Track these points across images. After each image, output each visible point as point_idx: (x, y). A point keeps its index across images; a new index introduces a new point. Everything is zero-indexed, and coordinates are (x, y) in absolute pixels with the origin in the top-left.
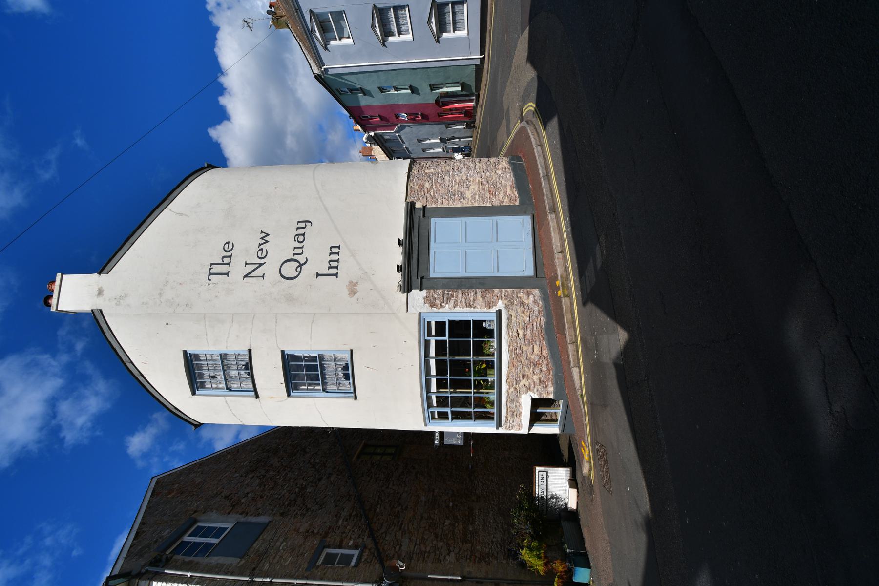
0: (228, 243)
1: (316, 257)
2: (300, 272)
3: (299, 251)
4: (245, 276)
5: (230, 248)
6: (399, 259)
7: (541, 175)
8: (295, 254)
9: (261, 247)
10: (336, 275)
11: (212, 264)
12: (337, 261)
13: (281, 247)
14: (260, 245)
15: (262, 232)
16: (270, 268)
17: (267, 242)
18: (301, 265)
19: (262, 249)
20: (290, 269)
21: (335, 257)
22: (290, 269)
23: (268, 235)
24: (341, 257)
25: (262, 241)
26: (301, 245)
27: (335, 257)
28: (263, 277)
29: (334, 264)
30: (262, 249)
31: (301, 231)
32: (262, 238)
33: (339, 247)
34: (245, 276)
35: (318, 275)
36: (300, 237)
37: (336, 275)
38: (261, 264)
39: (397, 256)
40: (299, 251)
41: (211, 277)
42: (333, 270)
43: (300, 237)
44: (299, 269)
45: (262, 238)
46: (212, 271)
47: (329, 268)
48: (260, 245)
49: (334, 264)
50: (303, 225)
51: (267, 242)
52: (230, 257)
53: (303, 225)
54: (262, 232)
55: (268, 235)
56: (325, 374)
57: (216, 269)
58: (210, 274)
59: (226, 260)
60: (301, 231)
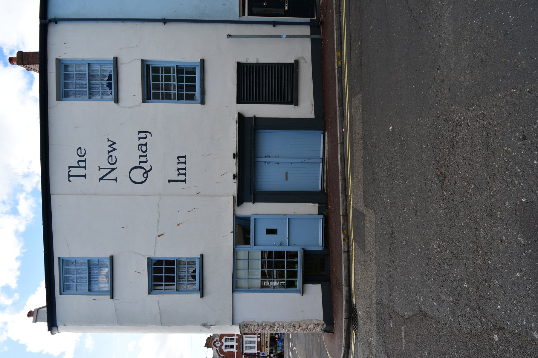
0: (80, 148)
1: (163, 166)
2: (147, 178)
3: (144, 159)
4: (101, 179)
5: (114, 162)
6: (234, 170)
7: (340, 178)
8: (140, 162)
9: (110, 154)
10: (185, 181)
11: (70, 167)
12: (185, 169)
13: (128, 155)
14: (109, 152)
15: (108, 140)
16: (122, 171)
17: (115, 149)
18: (147, 172)
19: (111, 156)
20: (138, 175)
21: (182, 166)
22: (138, 175)
23: (114, 143)
24: (187, 166)
25: (110, 149)
26: (145, 154)
27: (182, 166)
28: (116, 180)
29: (182, 172)
30: (111, 156)
31: (143, 142)
32: (110, 146)
33: (185, 157)
34: (101, 179)
35: (169, 181)
36: (143, 148)
37: (185, 181)
38: (113, 169)
39: (232, 166)
40: (144, 159)
41: (71, 178)
42: (181, 176)
43: (143, 148)
44: (145, 175)
45: (110, 146)
46: (71, 174)
47: (179, 175)
48: (109, 152)
49: (182, 172)
50: (143, 135)
51: (115, 149)
52: (85, 161)
53: (143, 135)
54: (108, 140)
55: (114, 143)
56: (68, 279)
57: (74, 172)
58: (70, 176)
59: (82, 164)
60: (143, 142)
